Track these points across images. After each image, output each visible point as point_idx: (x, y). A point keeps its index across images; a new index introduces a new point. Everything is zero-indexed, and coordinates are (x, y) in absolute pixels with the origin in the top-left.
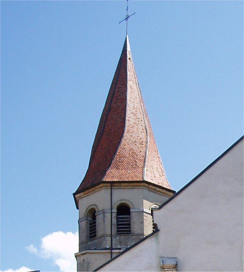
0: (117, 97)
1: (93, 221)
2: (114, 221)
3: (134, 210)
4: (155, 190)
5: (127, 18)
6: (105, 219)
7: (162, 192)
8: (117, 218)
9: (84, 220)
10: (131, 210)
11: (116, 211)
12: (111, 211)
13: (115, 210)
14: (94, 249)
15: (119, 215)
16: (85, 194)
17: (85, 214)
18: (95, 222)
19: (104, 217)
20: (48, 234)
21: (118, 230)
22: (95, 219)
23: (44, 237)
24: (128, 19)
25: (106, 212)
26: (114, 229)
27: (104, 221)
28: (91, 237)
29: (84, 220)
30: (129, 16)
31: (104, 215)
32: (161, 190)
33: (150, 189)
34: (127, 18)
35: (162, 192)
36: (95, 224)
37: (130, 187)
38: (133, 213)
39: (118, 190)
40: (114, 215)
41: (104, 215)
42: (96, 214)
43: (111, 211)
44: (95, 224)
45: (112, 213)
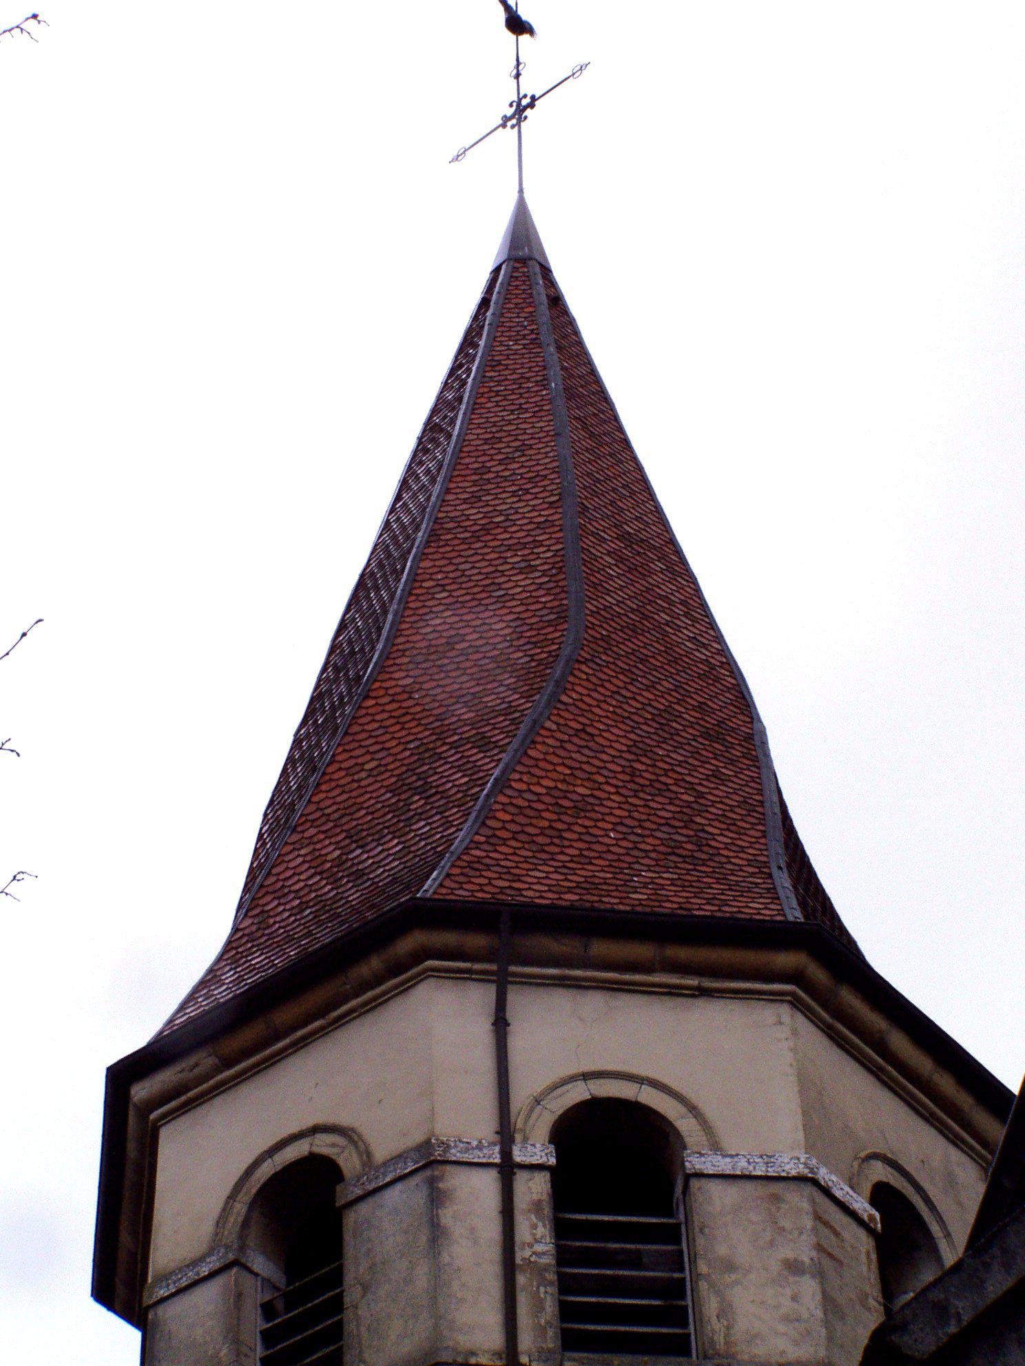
3: (724, 1165)
5: (521, 109)
6: (447, 1216)
8: (561, 1230)
9: (212, 1275)
11: (553, 1161)
12: (506, 1154)
15: (564, 1267)
16: (228, 1063)
17: (221, 1221)
19: (436, 1198)
21: (563, 1298)
23: (346, 1128)
24: (528, 112)
25: (454, 1155)
26: (539, 1306)
27: (437, 1233)
29: (212, 1275)
30: (534, 99)
31: (432, 1183)
34: (521, 109)
37: (674, 980)
38: (714, 1187)
39: (561, 1000)
41: (432, 1183)
43: (506, 1154)
45: (507, 1169)
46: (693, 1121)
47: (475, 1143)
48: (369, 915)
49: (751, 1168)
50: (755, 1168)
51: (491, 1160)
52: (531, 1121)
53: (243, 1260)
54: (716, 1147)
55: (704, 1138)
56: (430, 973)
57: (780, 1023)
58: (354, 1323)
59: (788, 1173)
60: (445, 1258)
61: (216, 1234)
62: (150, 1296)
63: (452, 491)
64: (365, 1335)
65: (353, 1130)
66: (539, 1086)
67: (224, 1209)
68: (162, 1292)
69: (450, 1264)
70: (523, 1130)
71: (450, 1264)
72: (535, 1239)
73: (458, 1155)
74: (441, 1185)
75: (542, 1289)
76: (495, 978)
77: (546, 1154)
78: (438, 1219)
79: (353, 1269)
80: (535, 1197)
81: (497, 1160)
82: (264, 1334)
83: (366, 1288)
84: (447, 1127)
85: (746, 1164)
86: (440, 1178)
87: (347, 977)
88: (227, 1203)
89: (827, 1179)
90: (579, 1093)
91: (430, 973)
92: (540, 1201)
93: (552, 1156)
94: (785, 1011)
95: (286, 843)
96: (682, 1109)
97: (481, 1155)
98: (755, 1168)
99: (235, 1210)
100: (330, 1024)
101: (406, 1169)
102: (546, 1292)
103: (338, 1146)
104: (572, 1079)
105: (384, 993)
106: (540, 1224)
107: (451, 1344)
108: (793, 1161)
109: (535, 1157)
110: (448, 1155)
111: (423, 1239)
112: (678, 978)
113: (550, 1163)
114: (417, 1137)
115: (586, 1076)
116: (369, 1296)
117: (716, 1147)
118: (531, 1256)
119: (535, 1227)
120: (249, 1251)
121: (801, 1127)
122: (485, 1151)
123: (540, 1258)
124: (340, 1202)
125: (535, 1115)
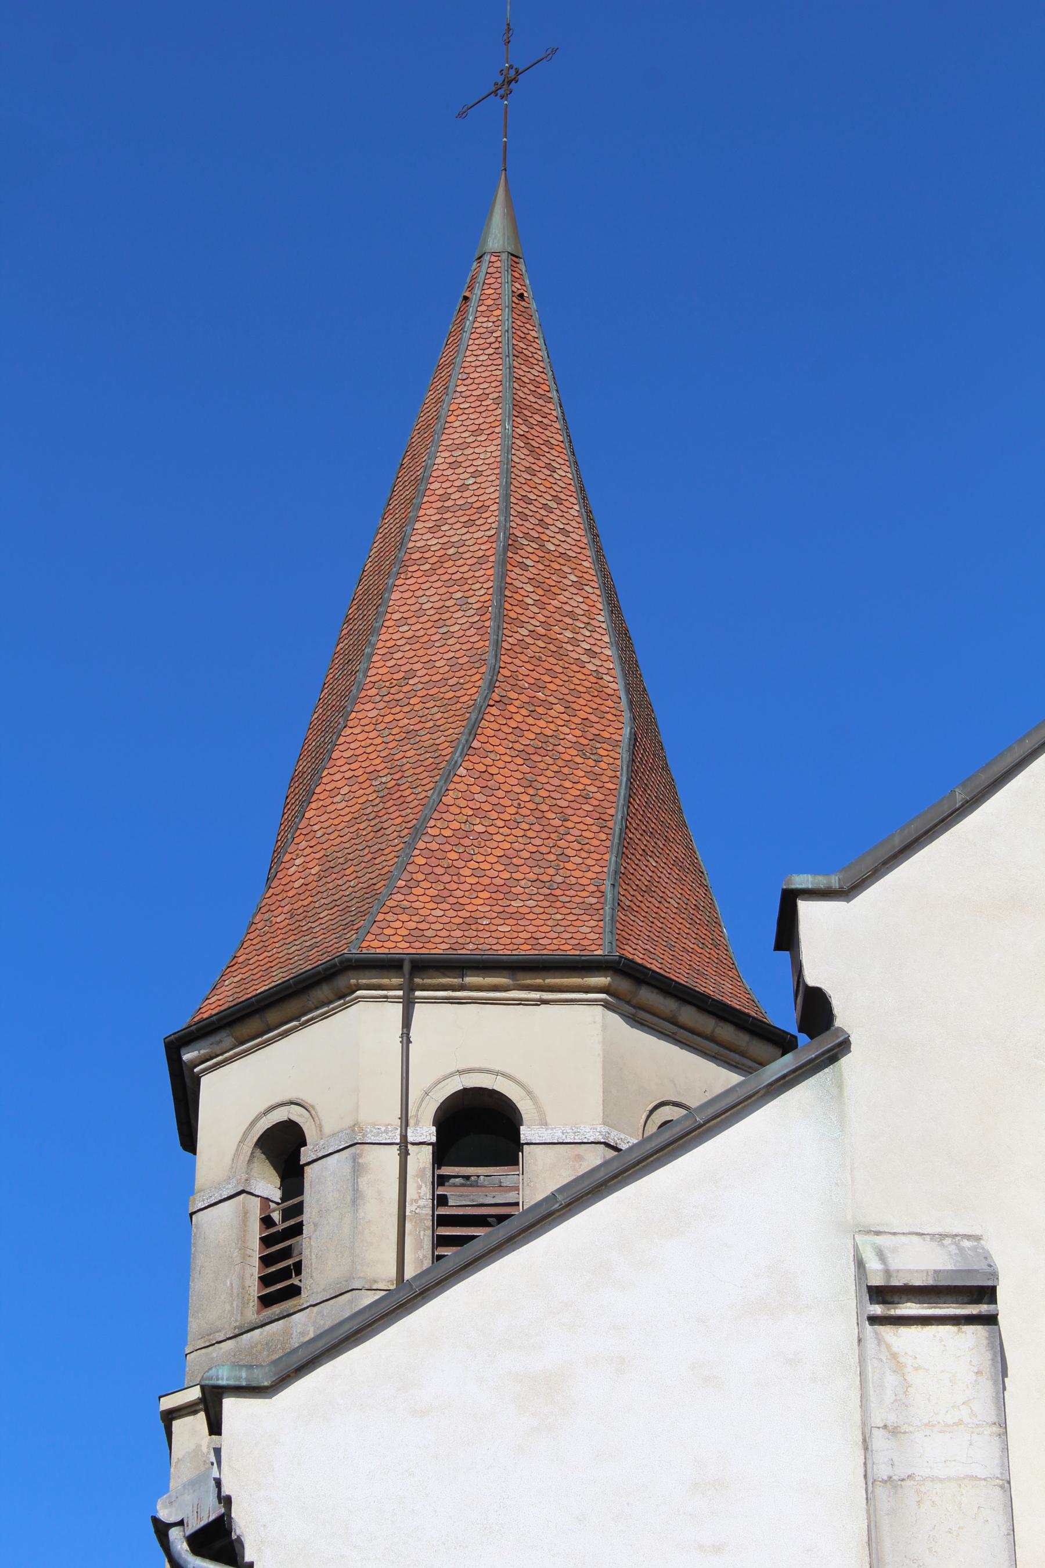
0: (446, 497)
1: (284, 1199)
2: (420, 1193)
4: (674, 1022)
5: (509, 81)
6: (363, 1182)
7: (711, 1039)
10: (526, 1133)
12: (404, 1137)
13: (425, 1131)
14: (762, 1096)
18: (301, 1203)
19: (357, 1169)
20: (442, 1206)
22: (301, 1192)
26: (419, 1246)
27: (356, 1197)
28: (266, 1301)
31: (355, 1158)
32: (696, 1047)
33: (643, 1015)
34: (509, 81)
35: (711, 1039)
36: (297, 1220)
40: (421, 1159)
41: (355, 1158)
42: (306, 1154)
43: (404, 1137)
44: (297, 1220)
45: (404, 1147)
46: (530, 1102)
47: (383, 1129)
48: (192, 1256)
49: (564, 1137)
50: (566, 1137)
51: (394, 1141)
52: (421, 1110)
53: (248, 1189)
54: (544, 1123)
55: (536, 1115)
56: (360, 999)
57: (595, 1022)
58: (309, 1250)
59: (588, 1139)
60: (361, 1214)
61: (233, 1167)
62: (193, 1207)
63: (421, 519)
64: (314, 1260)
65: (312, 1106)
66: (426, 1085)
67: (237, 1150)
68: (200, 1204)
69: (363, 1218)
70: (416, 1116)
71: (363, 1218)
72: (419, 1197)
73: (372, 1138)
74: (360, 1161)
75: (422, 1233)
76: (402, 1000)
77: (430, 1134)
78: (358, 1185)
79: (309, 1210)
80: (422, 1166)
81: (398, 1141)
82: (263, 1240)
83: (316, 1225)
84: (365, 1116)
85: (561, 1134)
86: (361, 1156)
87: (309, 996)
88: (239, 1145)
89: (616, 1139)
90: (455, 1085)
91: (360, 999)
92: (424, 1168)
93: (433, 1135)
94: (598, 1011)
95: (264, 898)
96: (523, 1093)
97: (387, 1137)
98: (566, 1137)
99: (244, 1151)
100: (301, 1025)
101: (340, 1146)
102: (425, 1235)
103: (303, 1117)
104: (451, 1075)
105: (333, 1009)
106: (423, 1185)
107: (362, 1275)
108: (592, 1130)
109: (423, 1137)
110: (366, 1138)
111: (349, 1198)
112: (525, 994)
113: (432, 1141)
114: (348, 1122)
115: (460, 1072)
116: (317, 1233)
117: (544, 1123)
118: (416, 1209)
119: (420, 1187)
120: (252, 1181)
121: (601, 1103)
122: (390, 1134)
123: (422, 1210)
124: (302, 1163)
125: (424, 1104)
